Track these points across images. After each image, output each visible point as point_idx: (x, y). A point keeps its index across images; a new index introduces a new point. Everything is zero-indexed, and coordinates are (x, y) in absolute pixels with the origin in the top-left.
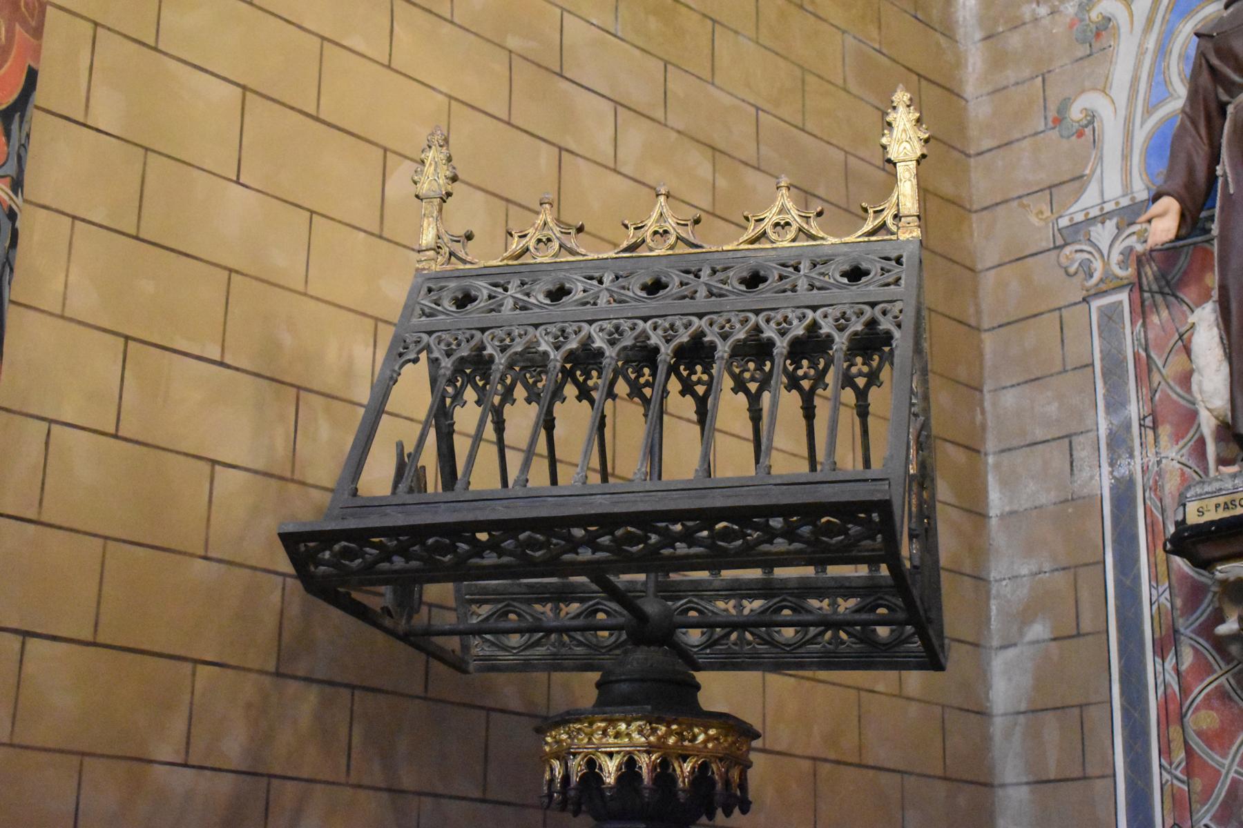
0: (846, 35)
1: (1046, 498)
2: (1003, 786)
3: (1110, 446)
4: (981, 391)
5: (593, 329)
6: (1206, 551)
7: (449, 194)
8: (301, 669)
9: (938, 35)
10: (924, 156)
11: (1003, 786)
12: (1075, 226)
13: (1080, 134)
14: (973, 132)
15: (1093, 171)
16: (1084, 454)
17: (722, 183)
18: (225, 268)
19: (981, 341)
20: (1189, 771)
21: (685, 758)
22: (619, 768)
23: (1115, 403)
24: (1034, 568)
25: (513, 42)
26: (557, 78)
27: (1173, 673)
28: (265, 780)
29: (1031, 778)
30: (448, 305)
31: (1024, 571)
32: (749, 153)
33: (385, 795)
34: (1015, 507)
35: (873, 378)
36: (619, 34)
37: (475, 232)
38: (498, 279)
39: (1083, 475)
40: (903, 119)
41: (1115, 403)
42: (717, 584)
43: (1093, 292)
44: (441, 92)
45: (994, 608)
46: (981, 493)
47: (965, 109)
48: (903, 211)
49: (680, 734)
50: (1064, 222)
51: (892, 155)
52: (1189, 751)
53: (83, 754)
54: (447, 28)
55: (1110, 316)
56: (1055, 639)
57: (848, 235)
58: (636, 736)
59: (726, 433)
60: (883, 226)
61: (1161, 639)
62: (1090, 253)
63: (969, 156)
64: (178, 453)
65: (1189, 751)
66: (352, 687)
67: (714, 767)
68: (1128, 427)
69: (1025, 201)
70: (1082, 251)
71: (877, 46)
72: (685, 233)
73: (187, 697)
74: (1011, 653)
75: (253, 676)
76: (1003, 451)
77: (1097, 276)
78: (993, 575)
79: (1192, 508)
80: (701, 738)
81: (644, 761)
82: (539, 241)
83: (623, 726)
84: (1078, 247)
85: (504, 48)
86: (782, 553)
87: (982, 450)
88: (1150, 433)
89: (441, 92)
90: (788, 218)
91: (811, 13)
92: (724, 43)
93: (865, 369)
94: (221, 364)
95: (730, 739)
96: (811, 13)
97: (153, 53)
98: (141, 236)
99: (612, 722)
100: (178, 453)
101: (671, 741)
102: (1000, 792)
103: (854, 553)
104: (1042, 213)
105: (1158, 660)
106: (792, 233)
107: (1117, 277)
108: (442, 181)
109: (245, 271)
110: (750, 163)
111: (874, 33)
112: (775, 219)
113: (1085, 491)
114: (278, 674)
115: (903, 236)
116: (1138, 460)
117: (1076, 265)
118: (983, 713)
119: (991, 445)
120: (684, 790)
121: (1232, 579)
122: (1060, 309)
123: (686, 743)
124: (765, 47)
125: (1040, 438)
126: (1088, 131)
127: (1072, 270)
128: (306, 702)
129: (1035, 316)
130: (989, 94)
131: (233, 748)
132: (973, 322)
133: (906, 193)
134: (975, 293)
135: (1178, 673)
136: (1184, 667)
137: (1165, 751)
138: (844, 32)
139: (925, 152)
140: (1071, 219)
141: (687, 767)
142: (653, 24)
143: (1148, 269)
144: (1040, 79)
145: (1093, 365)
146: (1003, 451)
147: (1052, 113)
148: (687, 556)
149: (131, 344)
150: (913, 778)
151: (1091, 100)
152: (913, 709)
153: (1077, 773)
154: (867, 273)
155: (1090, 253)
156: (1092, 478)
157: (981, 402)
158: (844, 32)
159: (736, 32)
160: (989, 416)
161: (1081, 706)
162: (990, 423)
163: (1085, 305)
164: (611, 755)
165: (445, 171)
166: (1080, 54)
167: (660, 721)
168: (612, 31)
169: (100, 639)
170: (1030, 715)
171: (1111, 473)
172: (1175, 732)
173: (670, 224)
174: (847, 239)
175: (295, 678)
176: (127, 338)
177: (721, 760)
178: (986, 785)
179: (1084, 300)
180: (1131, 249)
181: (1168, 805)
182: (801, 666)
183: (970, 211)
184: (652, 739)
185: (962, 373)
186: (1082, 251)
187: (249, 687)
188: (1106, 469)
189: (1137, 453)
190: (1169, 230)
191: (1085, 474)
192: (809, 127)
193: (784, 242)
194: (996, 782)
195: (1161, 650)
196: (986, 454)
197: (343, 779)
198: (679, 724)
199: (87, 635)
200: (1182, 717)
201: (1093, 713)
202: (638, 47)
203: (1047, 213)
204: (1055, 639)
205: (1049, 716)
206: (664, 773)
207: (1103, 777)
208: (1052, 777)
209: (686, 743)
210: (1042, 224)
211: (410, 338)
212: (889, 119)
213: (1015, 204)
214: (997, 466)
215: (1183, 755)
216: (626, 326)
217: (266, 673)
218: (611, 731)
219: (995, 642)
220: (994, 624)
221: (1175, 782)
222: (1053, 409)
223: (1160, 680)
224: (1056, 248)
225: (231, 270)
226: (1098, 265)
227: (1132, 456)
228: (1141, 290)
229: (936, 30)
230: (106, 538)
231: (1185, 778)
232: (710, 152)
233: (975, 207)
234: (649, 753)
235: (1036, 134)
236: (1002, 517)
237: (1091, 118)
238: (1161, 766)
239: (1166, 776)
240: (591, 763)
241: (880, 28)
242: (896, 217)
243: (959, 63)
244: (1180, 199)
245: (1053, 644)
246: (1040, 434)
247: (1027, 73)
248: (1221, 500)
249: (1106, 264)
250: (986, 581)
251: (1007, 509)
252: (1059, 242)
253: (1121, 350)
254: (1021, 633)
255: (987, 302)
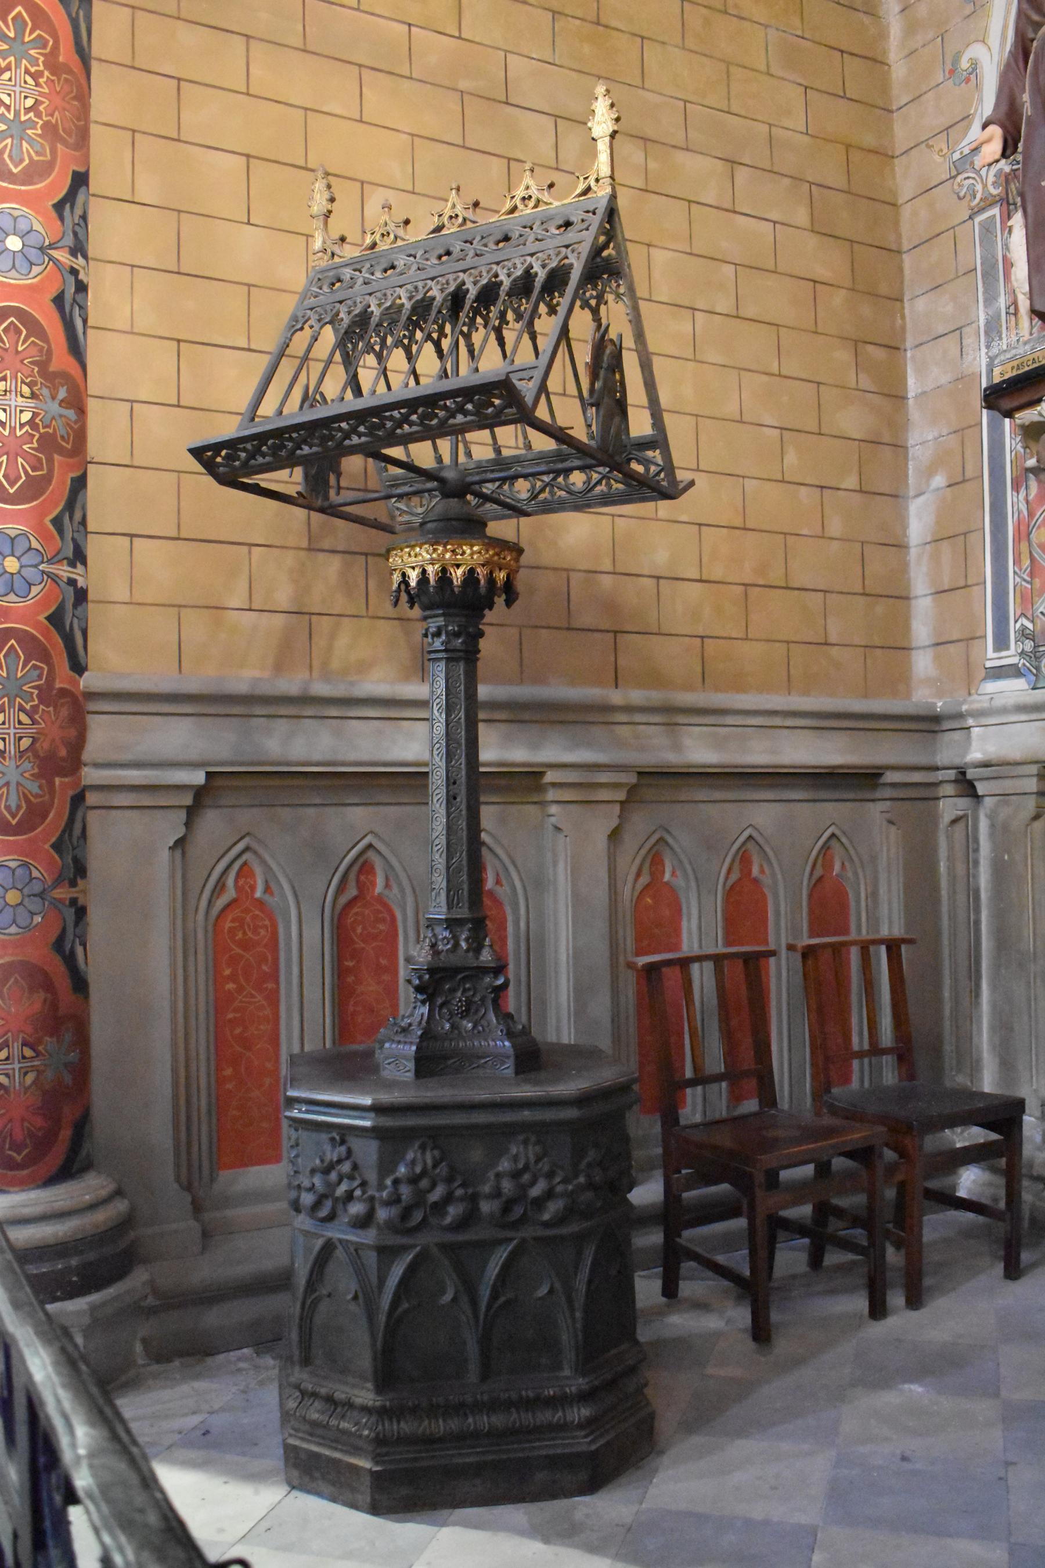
0: (768, 29)
1: (944, 379)
2: (916, 597)
3: (987, 333)
4: (901, 301)
5: (402, 292)
6: (1007, 404)
7: (330, 212)
8: (326, 544)
9: (861, 15)
10: (615, 132)
11: (916, 597)
12: (963, 157)
13: (968, 80)
14: (895, 91)
15: (976, 110)
16: (970, 341)
17: (652, 165)
18: (245, 284)
19: (902, 261)
20: (1032, 575)
21: (458, 566)
22: (418, 576)
23: (990, 299)
24: (936, 434)
25: (463, 85)
26: (503, 105)
27: (1024, 503)
28: (307, 617)
29: (933, 591)
30: (326, 289)
31: (930, 437)
32: (679, 138)
33: (396, 622)
34: (926, 389)
35: (600, 298)
36: (557, 62)
37: (346, 234)
38: (356, 265)
39: (968, 359)
40: (601, 106)
41: (990, 299)
42: (530, 457)
43: (976, 210)
44: (405, 133)
45: (910, 467)
46: (902, 380)
47: (889, 72)
48: (602, 175)
49: (453, 551)
50: (957, 156)
51: (595, 134)
52: (1032, 559)
53: (180, 606)
54: (407, 83)
55: (987, 229)
56: (949, 486)
57: (566, 198)
58: (424, 554)
59: (659, 355)
60: (588, 189)
61: (1017, 477)
62: (974, 178)
63: (891, 112)
64: (224, 412)
65: (1032, 559)
66: (366, 555)
67: (479, 570)
68: (999, 315)
69: (931, 142)
70: (968, 178)
71: (799, 33)
72: (469, 215)
73: (246, 569)
74: (921, 500)
75: (291, 553)
76: (917, 346)
77: (979, 196)
78: (911, 442)
79: (997, 371)
80: (468, 551)
81: (430, 569)
82: (383, 235)
83: (418, 549)
84: (966, 175)
85: (457, 90)
86: (462, 424)
87: (902, 347)
88: (1013, 318)
89: (405, 133)
90: (530, 193)
91: (734, 16)
92: (652, 53)
93: (594, 293)
94: (249, 350)
95: (491, 552)
96: (734, 16)
97: (557, 114)
98: (182, 271)
99: (413, 547)
100: (224, 412)
101: (448, 555)
102: (913, 602)
103: (503, 418)
104: (941, 150)
105: (1015, 494)
106: (531, 204)
107: (992, 196)
108: (324, 203)
109: (261, 284)
110: (679, 145)
111: (797, 22)
112: (523, 194)
113: (970, 371)
114: (309, 549)
115: (600, 194)
116: (1005, 341)
117: (965, 190)
118: (901, 546)
119: (909, 343)
120: (458, 586)
121: (1027, 424)
122: (953, 228)
123: (459, 557)
124: (691, 51)
125: (941, 331)
126: (973, 77)
127: (962, 194)
128: (333, 566)
129: (938, 235)
130: (906, 57)
131: (283, 597)
132: (894, 247)
133: (603, 163)
134: (896, 223)
135: (1027, 502)
136: (1031, 498)
137: (1017, 561)
138: (766, 26)
139: (616, 128)
140: (961, 153)
141: (460, 572)
142: (587, 49)
143: (1013, 186)
144: (940, 38)
145: (976, 269)
146: (917, 346)
147: (949, 67)
148: (411, 434)
149: (182, 344)
150: (834, 595)
151: (976, 51)
152: (835, 545)
153: (962, 583)
154: (559, 227)
155: (974, 178)
156: (975, 359)
157: (903, 308)
158: (766, 26)
159: (664, 43)
160: (908, 319)
161: (965, 534)
162: (909, 325)
163: (971, 222)
164: (413, 568)
165: (327, 195)
166: (967, 12)
167: (437, 543)
168: (551, 61)
169: (182, 536)
170: (933, 544)
171: (987, 353)
172: (1024, 546)
173: (459, 210)
174: (566, 202)
175: (323, 551)
176: (179, 341)
177: (483, 565)
178: (905, 598)
179: (970, 218)
180: (1001, 170)
181: (1018, 600)
182: (589, 506)
183: (893, 157)
184: (434, 556)
185: (884, 289)
186: (968, 178)
187: (290, 559)
188: (984, 350)
189: (1004, 336)
190: (995, 153)
191: (970, 358)
192: (734, 109)
193: (527, 211)
194: (912, 596)
195: (1016, 488)
196: (905, 350)
197: (365, 614)
198: (452, 545)
199: (174, 534)
200: (1029, 534)
201: (973, 538)
202: (574, 70)
203: (945, 151)
204: (949, 486)
205: (945, 543)
206: (444, 577)
207: (977, 584)
208: (946, 588)
209: (459, 557)
210: (942, 159)
211: (300, 314)
212: (593, 107)
213: (923, 146)
214: (913, 357)
215: (1028, 562)
216: (420, 284)
217: (303, 549)
218: (412, 553)
219: (912, 493)
220: (911, 481)
221: (1024, 583)
222: (950, 308)
223: (1015, 508)
224: (951, 178)
225: (249, 285)
226: (979, 187)
227: (1001, 339)
228: (1008, 204)
229: (858, 10)
230: (179, 472)
231: (1029, 579)
232: (641, 142)
233: (897, 153)
234: (433, 564)
235: (938, 85)
236: (916, 397)
237: (975, 65)
238: (1015, 572)
239: (1018, 579)
240: (404, 575)
241: (802, 19)
242: (597, 180)
243: (883, 35)
244: (1002, 126)
245: (948, 489)
246: (941, 330)
247: (931, 35)
248: (1015, 363)
249: (985, 186)
250: (905, 448)
251: (920, 391)
252: (954, 173)
253: (994, 257)
254: (928, 485)
255: (905, 228)
